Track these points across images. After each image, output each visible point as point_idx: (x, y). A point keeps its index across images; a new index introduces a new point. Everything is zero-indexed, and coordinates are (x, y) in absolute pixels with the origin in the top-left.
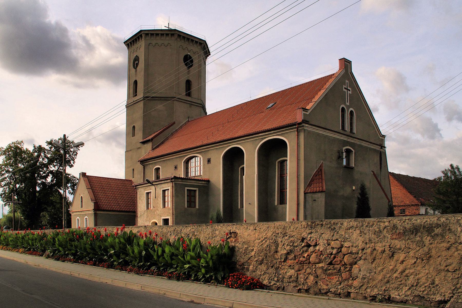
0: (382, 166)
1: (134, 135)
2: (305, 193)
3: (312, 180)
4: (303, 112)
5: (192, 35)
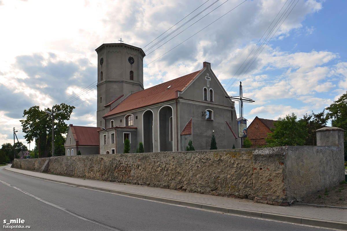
0: (233, 118)
4: (179, 93)
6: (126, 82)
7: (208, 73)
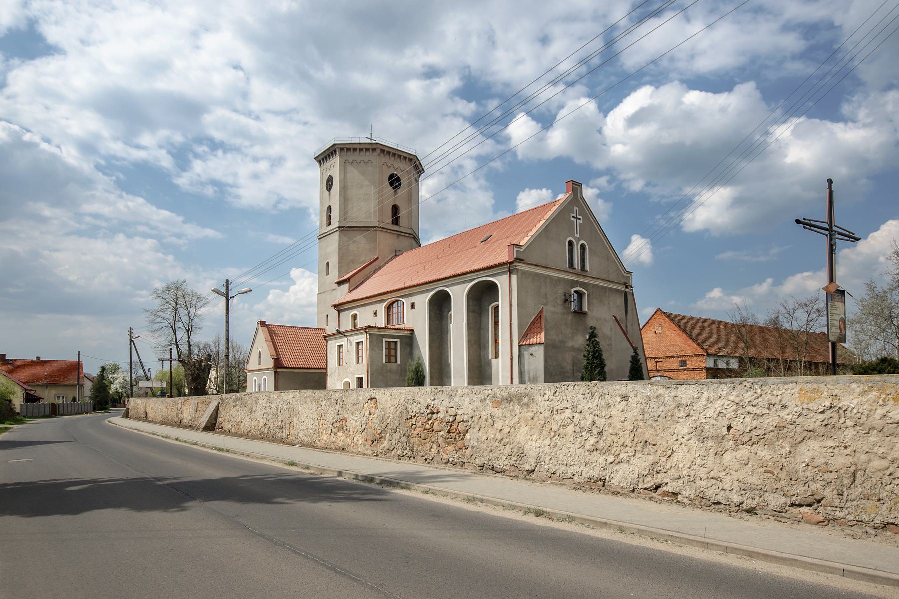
1: (327, 273)
2: (520, 346)
3: (530, 329)
4: (516, 249)
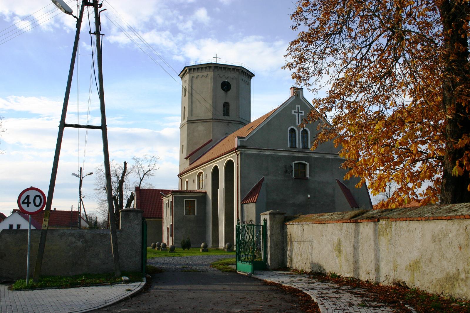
1: (183, 153)
5: (228, 64)
6: (216, 119)
7: (299, 105)
